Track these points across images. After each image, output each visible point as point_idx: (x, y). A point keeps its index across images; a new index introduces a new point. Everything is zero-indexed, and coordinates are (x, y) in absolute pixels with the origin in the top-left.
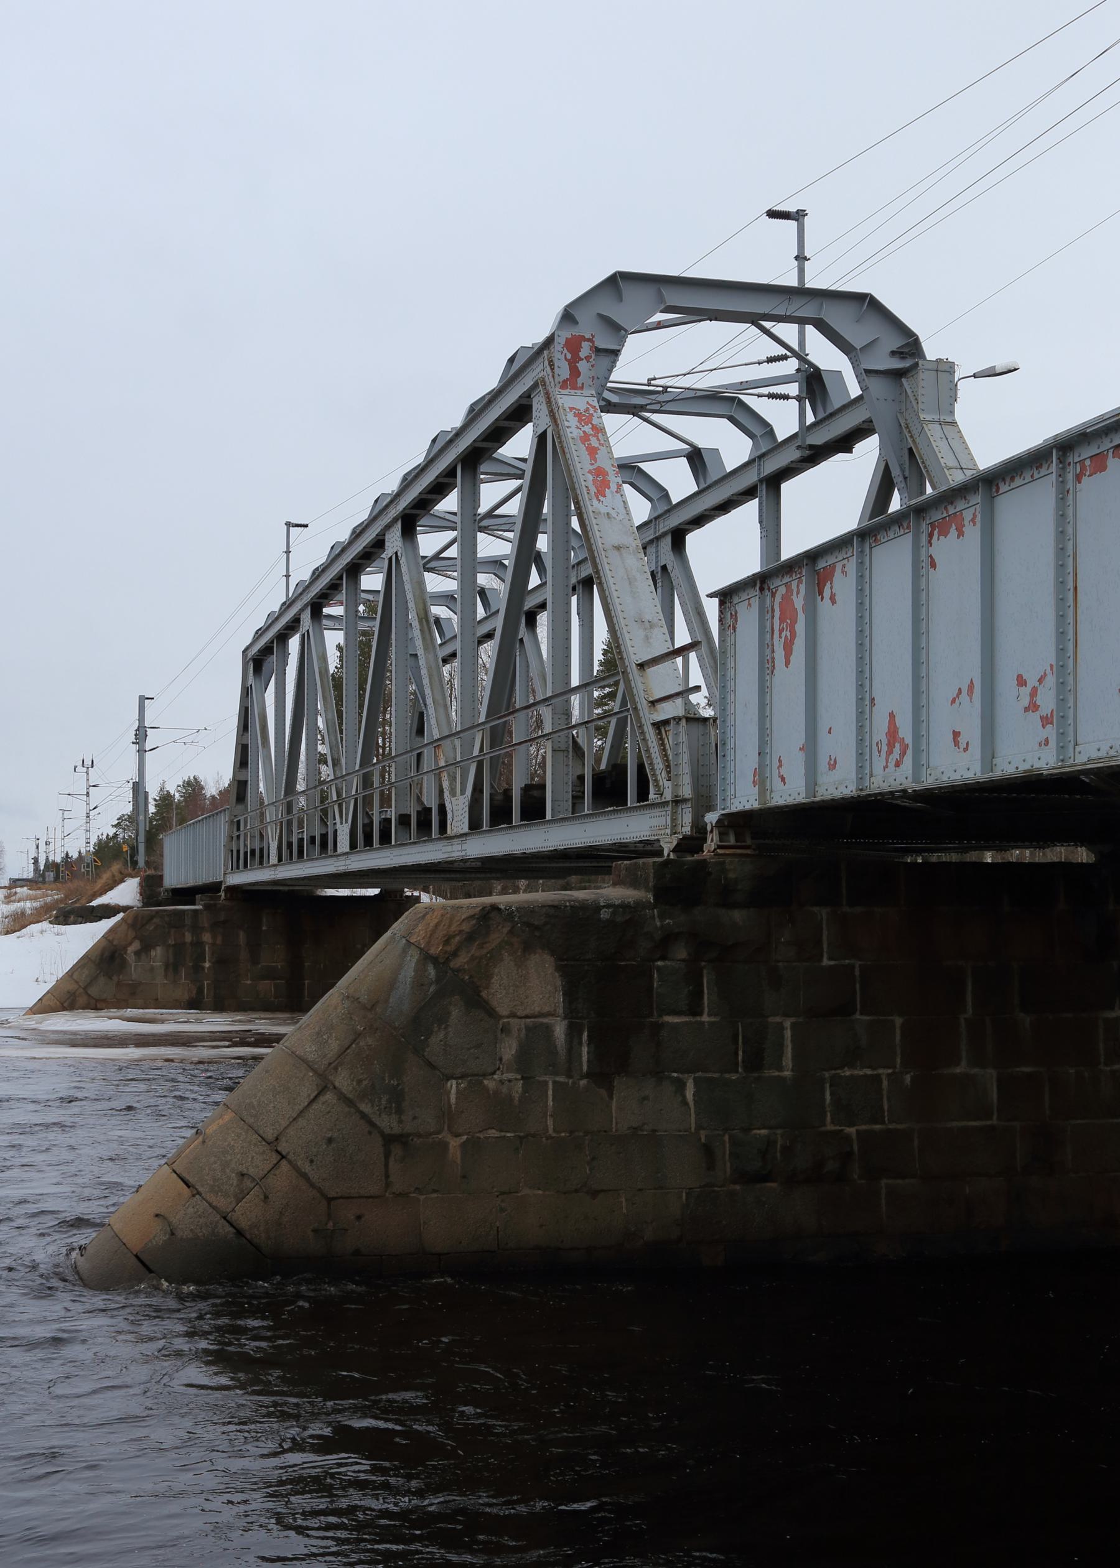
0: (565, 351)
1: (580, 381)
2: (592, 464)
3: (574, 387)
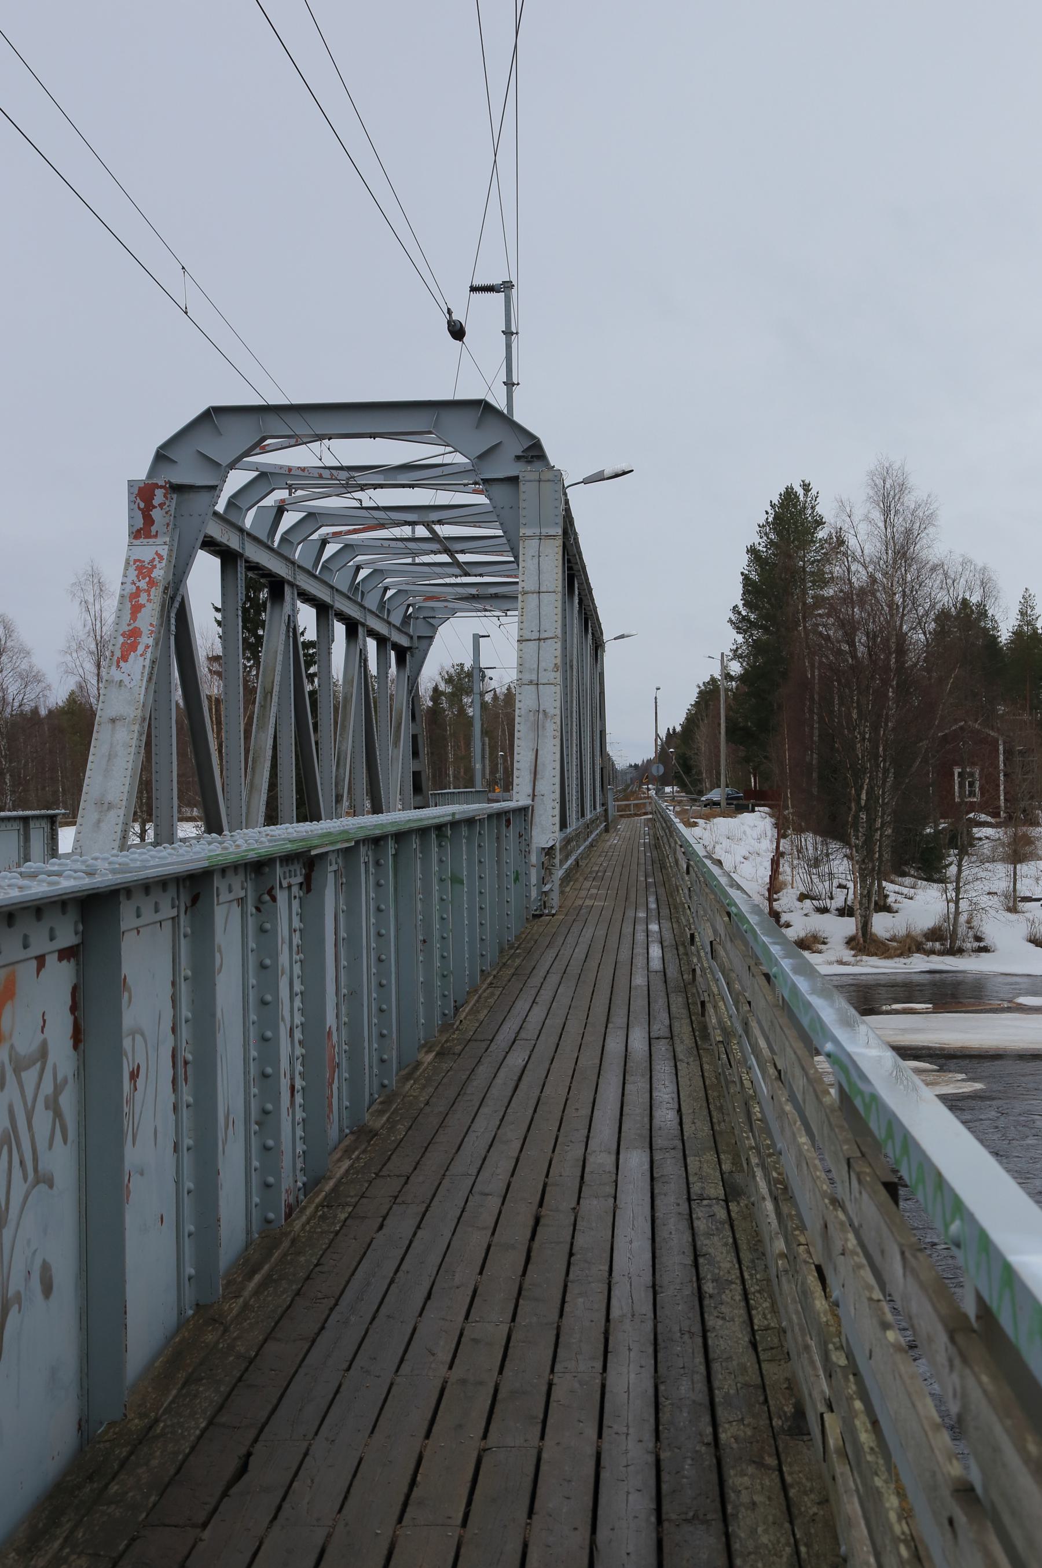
0: (139, 500)
1: (154, 529)
3: (148, 536)
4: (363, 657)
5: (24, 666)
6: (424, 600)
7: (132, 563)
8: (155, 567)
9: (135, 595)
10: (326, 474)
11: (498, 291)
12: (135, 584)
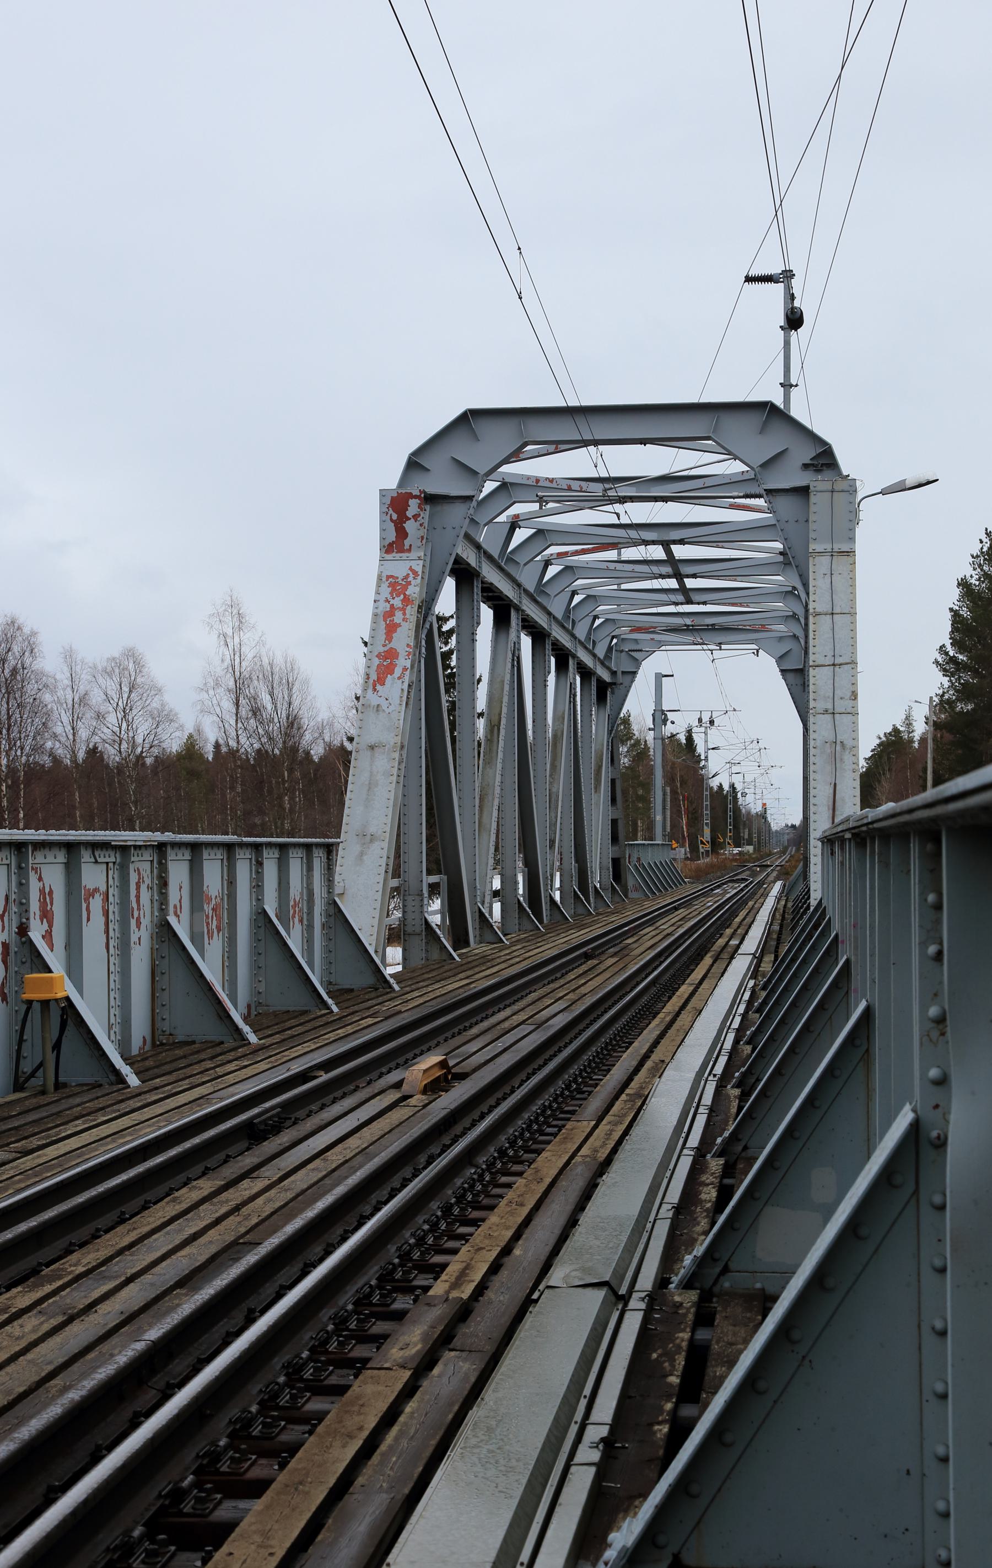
0: (391, 511)
1: (407, 543)
2: (384, 646)
3: (401, 550)
4: (573, 691)
5: (155, 704)
6: (631, 631)
7: (384, 579)
8: (409, 583)
9: (390, 613)
10: (575, 485)
11: (777, 282)
12: (389, 602)
